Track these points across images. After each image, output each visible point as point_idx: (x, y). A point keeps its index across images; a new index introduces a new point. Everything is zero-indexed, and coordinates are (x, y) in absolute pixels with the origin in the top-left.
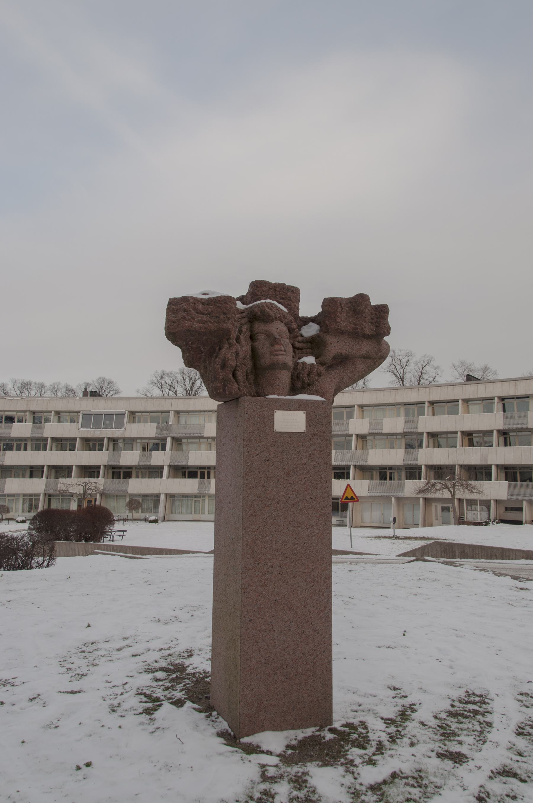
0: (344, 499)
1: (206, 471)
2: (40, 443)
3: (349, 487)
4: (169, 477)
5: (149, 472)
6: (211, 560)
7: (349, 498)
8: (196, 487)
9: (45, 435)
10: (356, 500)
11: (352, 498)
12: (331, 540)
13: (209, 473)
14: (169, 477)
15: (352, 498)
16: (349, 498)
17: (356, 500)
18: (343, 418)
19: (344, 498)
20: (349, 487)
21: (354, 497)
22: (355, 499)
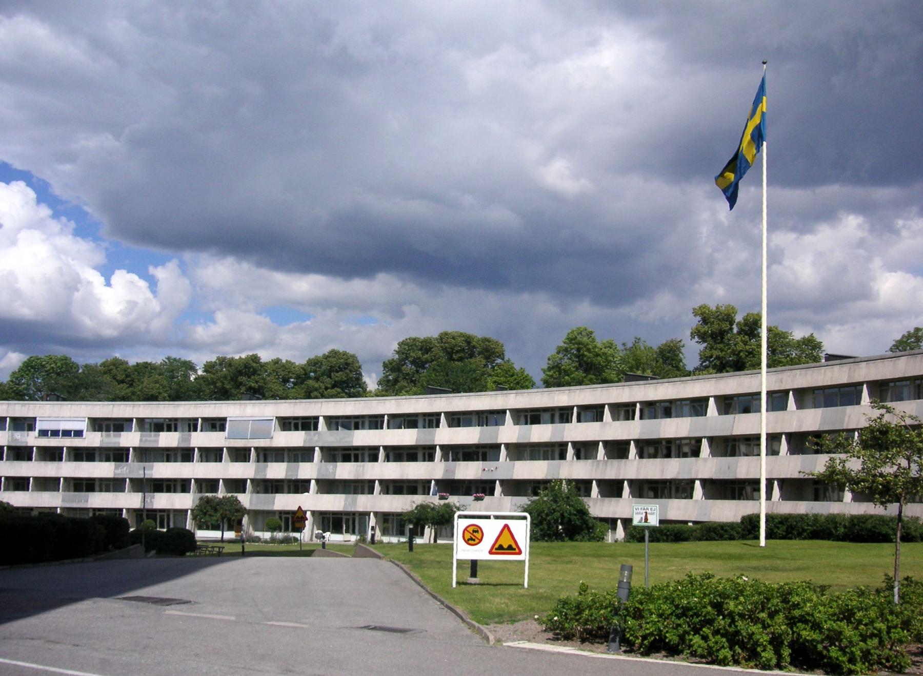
0: (496, 549)
1: (172, 484)
2: (311, 423)
3: (506, 529)
4: (134, 461)
5: (302, 454)
6: (142, 476)
7: (505, 546)
8: (343, 503)
9: (192, 445)
10: (517, 551)
11: (510, 547)
12: (425, 445)
13: (175, 485)
14: (134, 461)
15: (510, 547)
16: (505, 546)
17: (517, 551)
18: (769, 518)
19: (497, 546)
20: (506, 529)
21: (514, 546)
22: (515, 549)
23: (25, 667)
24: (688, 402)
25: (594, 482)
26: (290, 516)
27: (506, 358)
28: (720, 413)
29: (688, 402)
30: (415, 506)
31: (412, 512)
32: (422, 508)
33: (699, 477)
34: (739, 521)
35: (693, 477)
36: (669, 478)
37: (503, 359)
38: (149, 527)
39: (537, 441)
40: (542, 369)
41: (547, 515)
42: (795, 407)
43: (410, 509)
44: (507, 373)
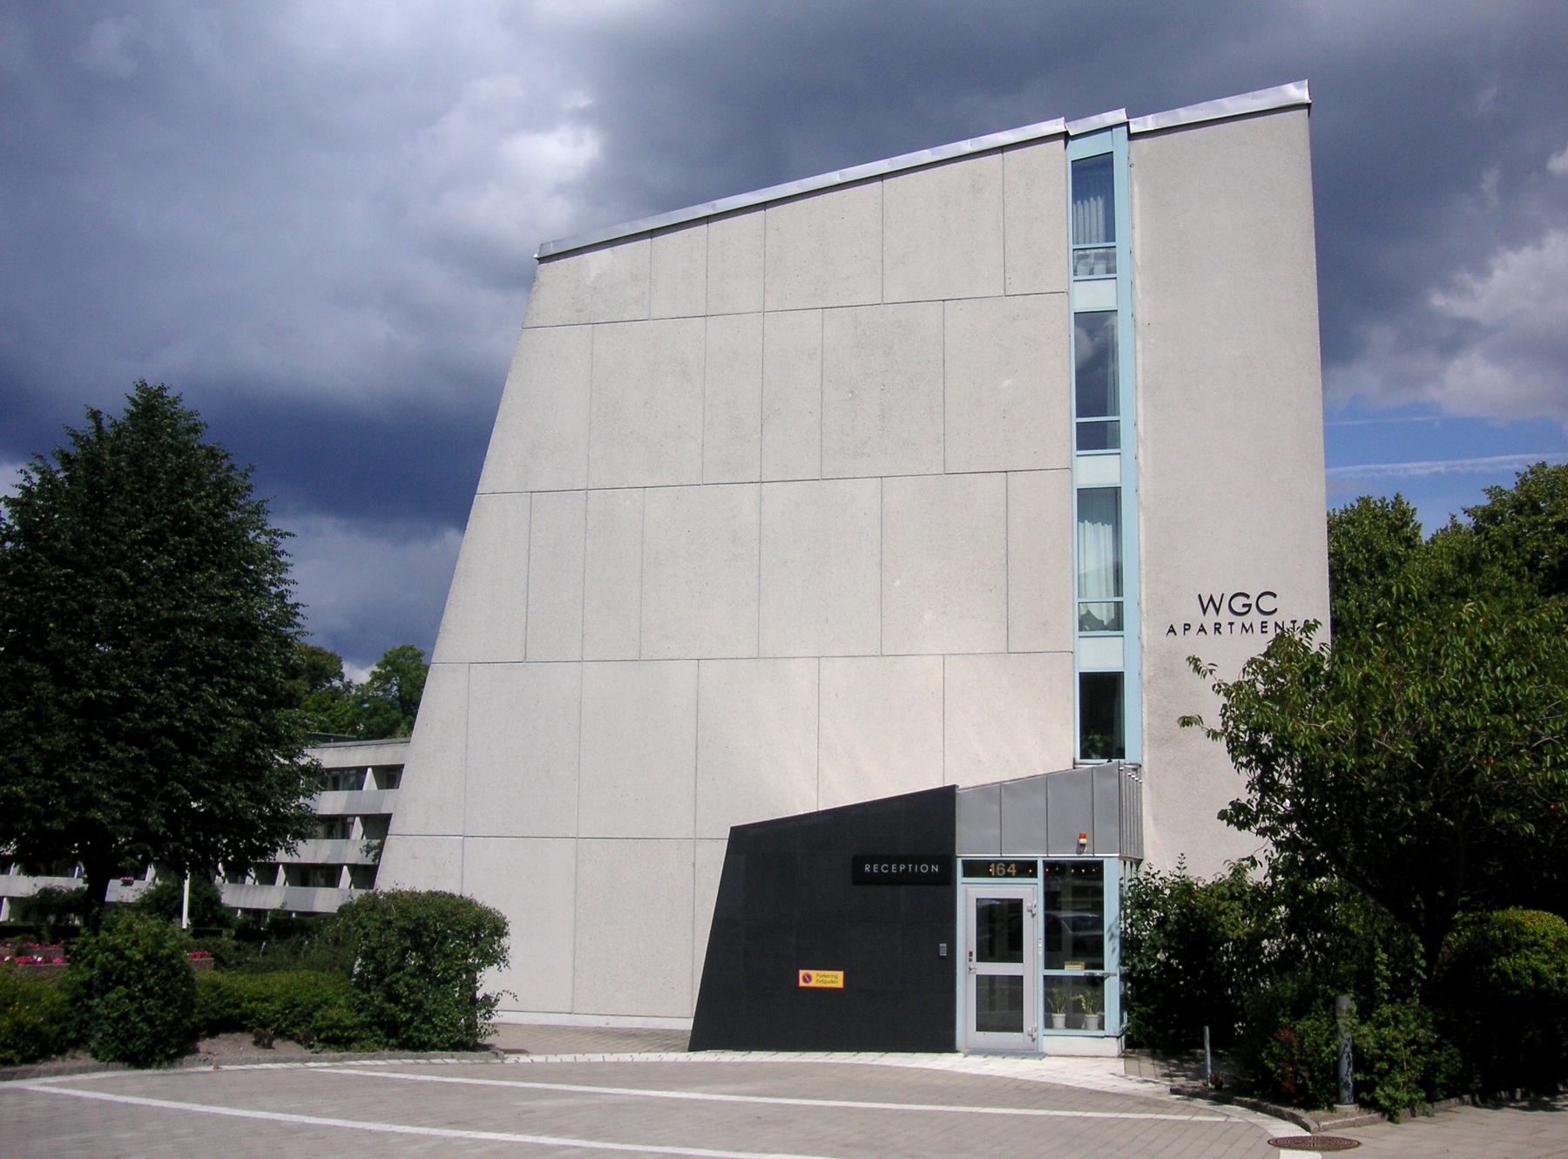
23: (162, 1108)
24: (355, 772)
25: (345, 868)
26: (1031, 893)
27: (346, 679)
28: (380, 787)
29: (355, 772)
30: (36, 891)
31: (33, 897)
32: (46, 893)
33: (347, 862)
34: (335, 911)
35: (341, 862)
36: (320, 862)
37: (341, 680)
38: (291, 913)
39: (329, 813)
40: (1223, 815)
41: (166, 903)
42: (376, 788)
43: (31, 894)
44: (319, 706)
